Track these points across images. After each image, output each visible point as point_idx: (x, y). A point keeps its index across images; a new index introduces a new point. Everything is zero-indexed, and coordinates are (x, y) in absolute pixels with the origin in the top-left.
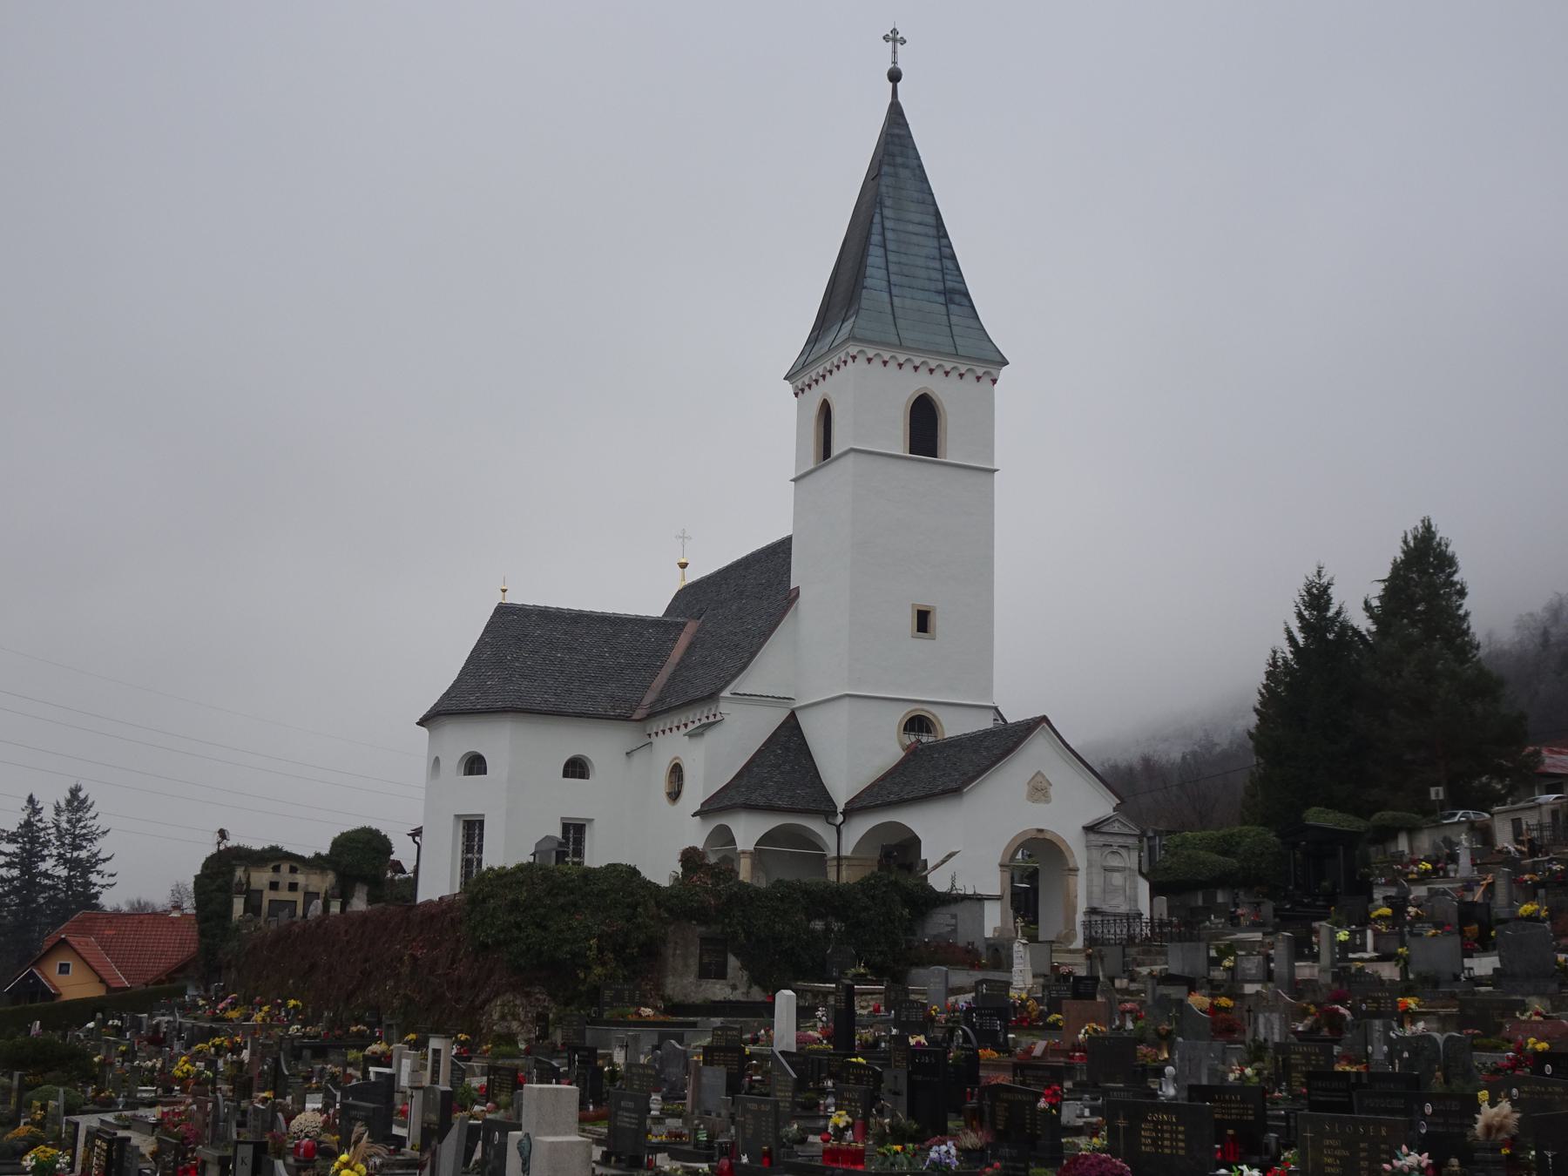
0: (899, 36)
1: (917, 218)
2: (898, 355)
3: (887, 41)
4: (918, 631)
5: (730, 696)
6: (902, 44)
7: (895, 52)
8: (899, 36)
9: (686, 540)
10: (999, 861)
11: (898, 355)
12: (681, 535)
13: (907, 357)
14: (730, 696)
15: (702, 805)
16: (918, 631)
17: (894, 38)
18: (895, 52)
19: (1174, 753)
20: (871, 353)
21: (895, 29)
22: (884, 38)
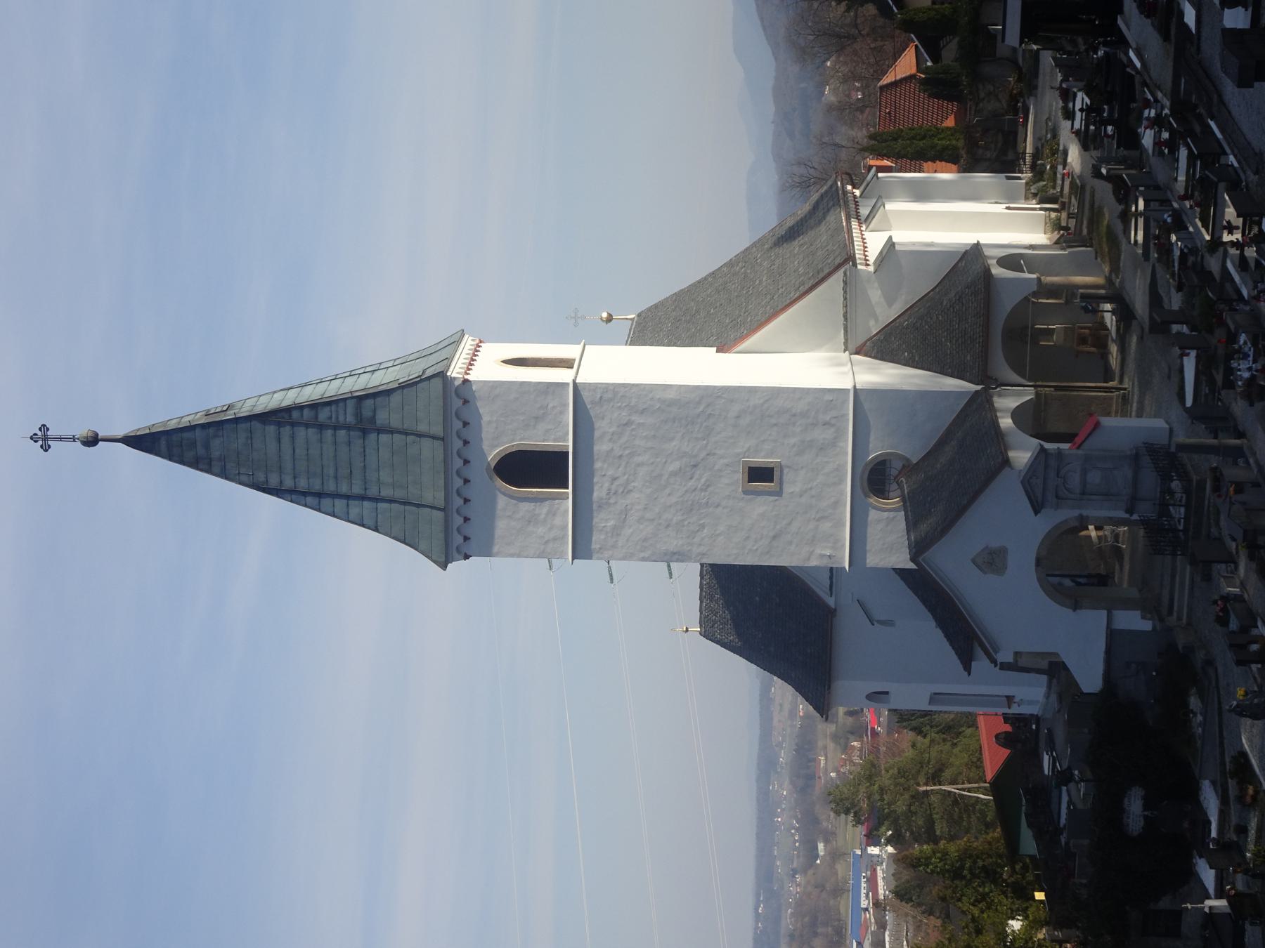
0: (40, 443)
1: (272, 446)
2: (455, 508)
3: (49, 447)
4: (749, 468)
5: (833, 598)
6: (48, 429)
7: (61, 439)
8: (40, 443)
9: (573, 315)
10: (1071, 611)
11: (455, 508)
12: (573, 321)
13: (455, 515)
14: (833, 598)
15: (910, 554)
16: (749, 468)
17: (43, 438)
18: (61, 439)
19: (770, 109)
20: (458, 520)
21: (31, 438)
22: (46, 451)
